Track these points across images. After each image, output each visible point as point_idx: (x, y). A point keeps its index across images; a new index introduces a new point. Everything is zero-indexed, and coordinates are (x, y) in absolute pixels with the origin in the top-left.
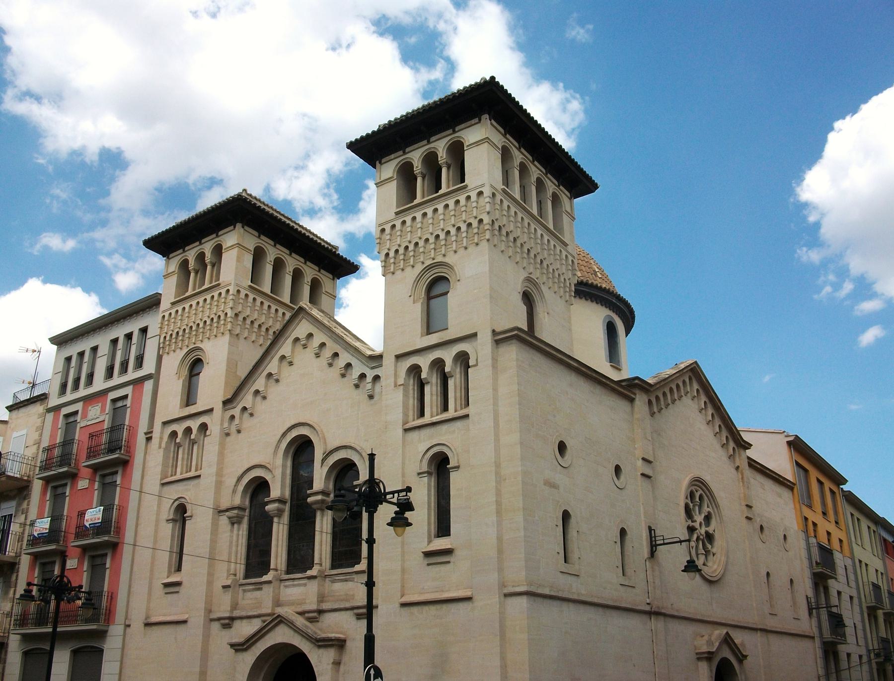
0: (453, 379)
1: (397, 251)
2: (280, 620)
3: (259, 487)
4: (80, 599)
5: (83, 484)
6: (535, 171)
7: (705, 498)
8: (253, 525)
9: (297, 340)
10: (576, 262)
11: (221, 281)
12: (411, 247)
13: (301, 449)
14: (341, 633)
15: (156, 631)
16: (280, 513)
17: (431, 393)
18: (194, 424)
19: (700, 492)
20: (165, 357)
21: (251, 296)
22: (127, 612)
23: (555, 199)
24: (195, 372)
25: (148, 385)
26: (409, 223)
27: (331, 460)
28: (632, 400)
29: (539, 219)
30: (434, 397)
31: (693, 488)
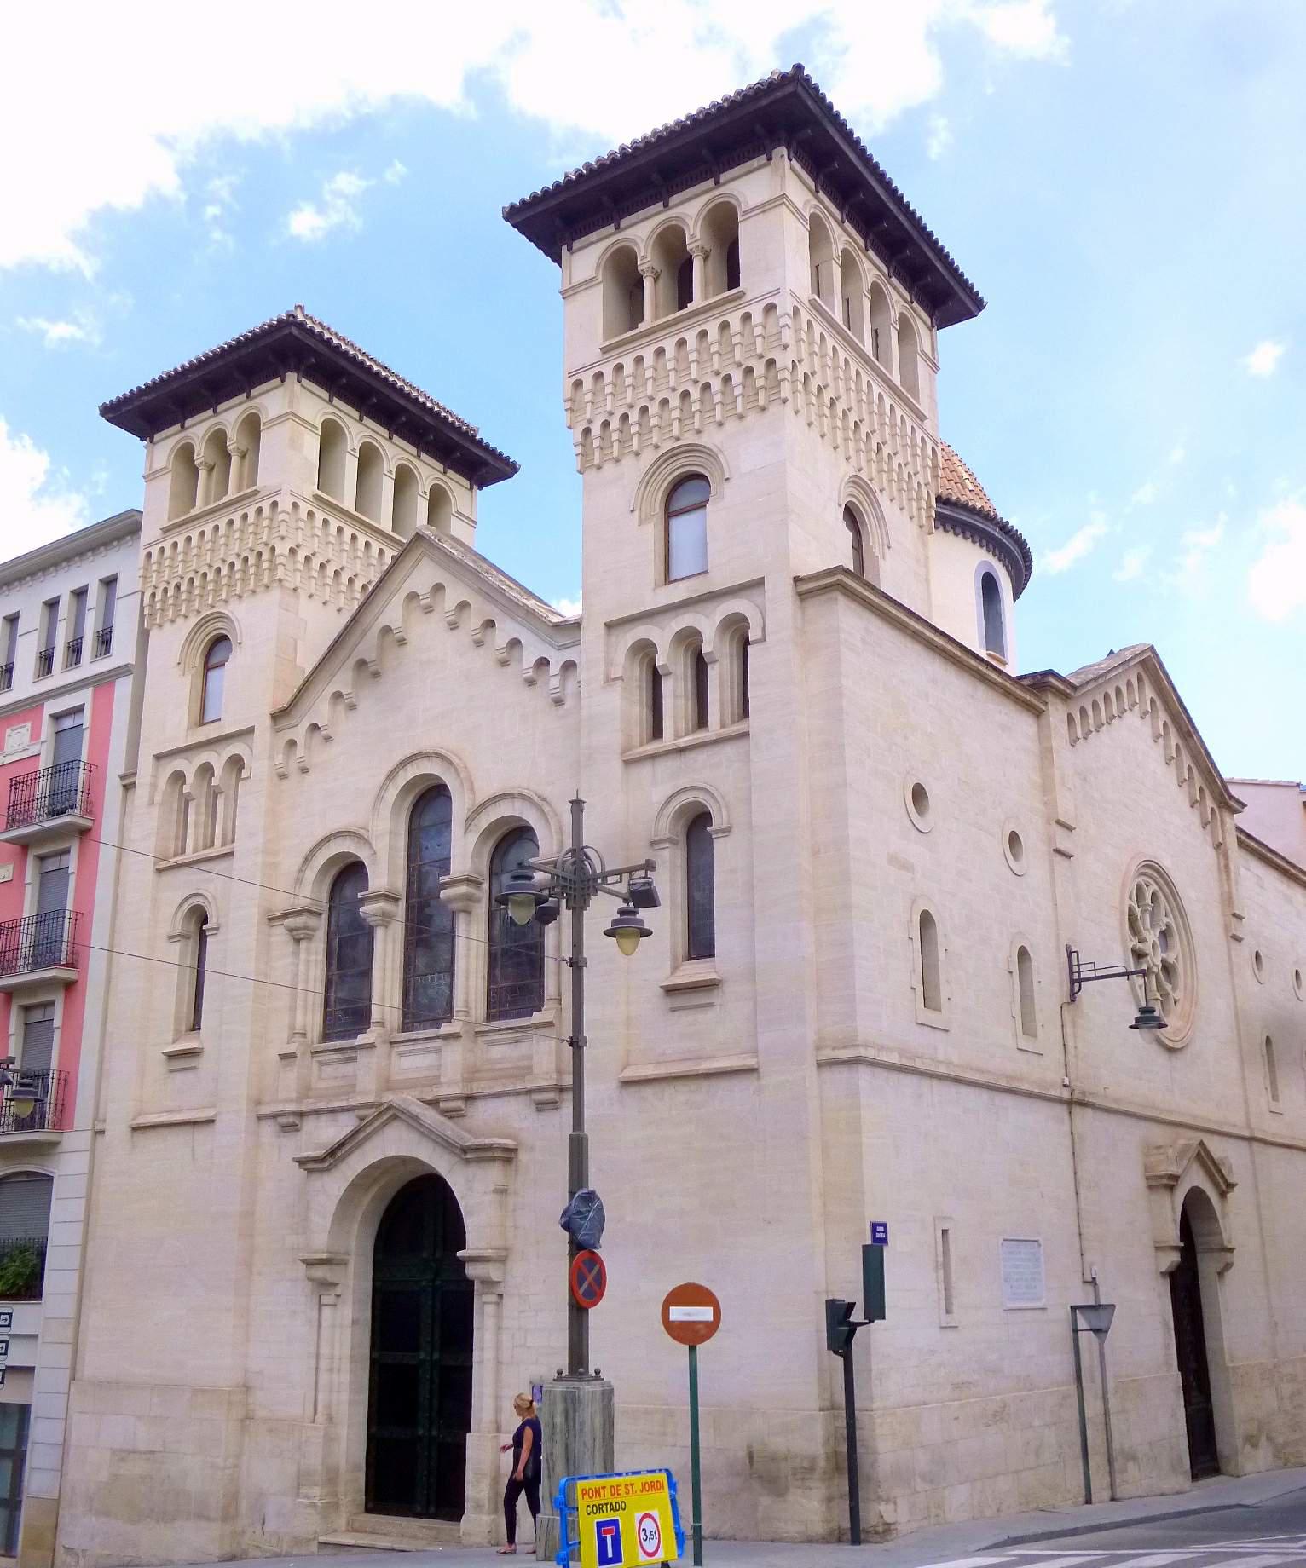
0: (717, 666)
1: (606, 424)
2: (391, 1114)
3: (349, 872)
4: (9, 1082)
6: (871, 268)
7: (1162, 898)
8: (335, 943)
9: (413, 596)
10: (938, 450)
11: (260, 483)
12: (634, 416)
13: (428, 801)
15: (153, 1141)
16: (387, 918)
17: (676, 695)
19: (1154, 887)
20: (154, 633)
21: (320, 516)
22: (97, 1108)
23: (905, 327)
24: (214, 660)
25: (123, 689)
26: (629, 368)
27: (485, 820)
28: (1038, 713)
29: (874, 363)
30: (681, 702)
31: (1142, 879)
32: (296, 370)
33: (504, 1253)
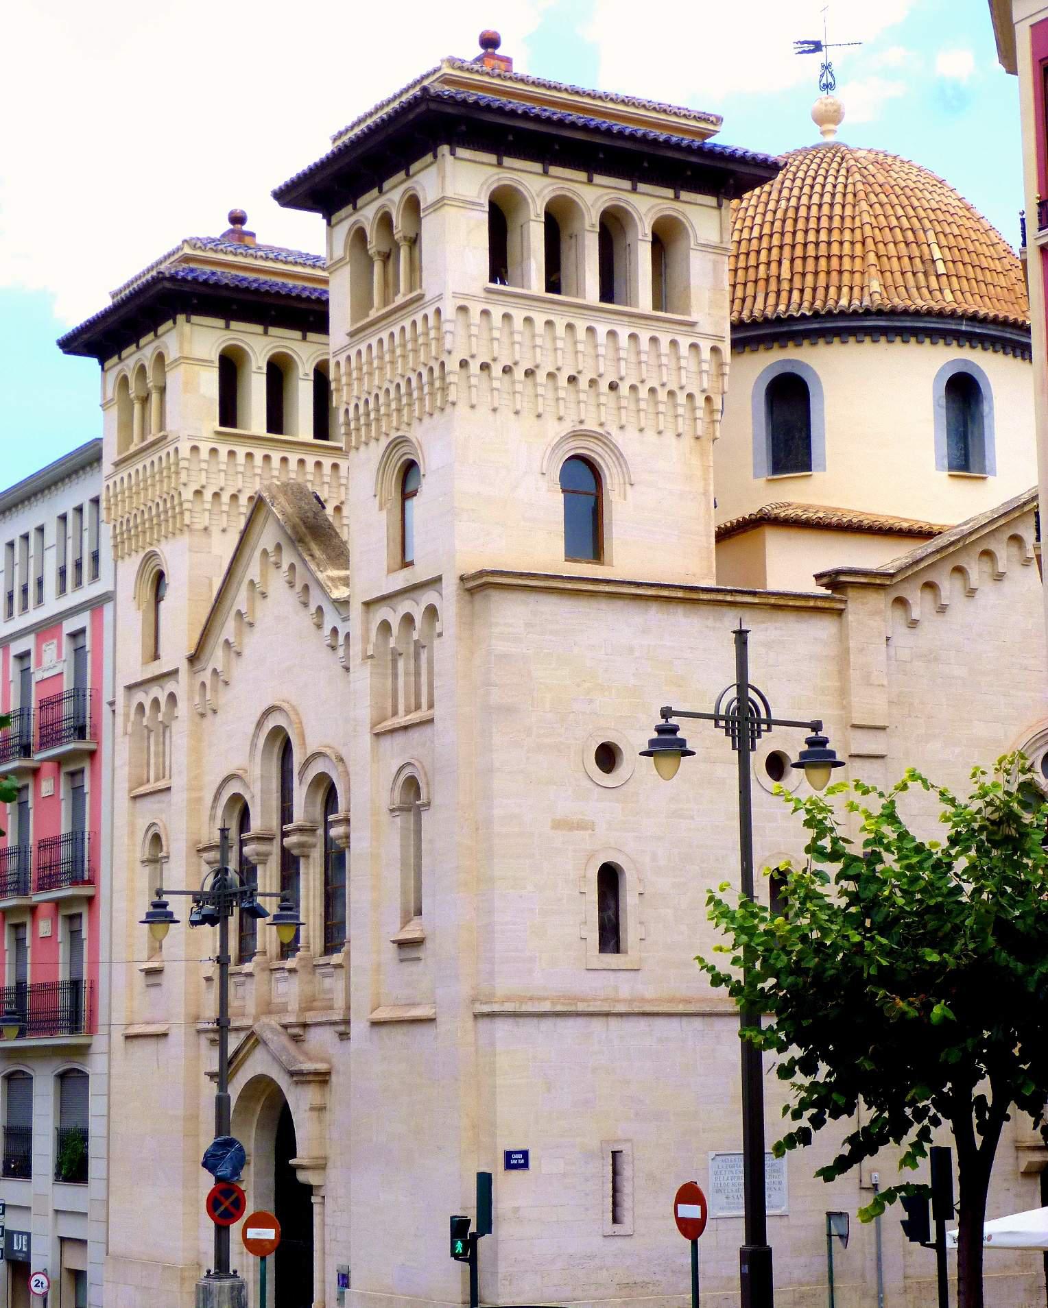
0: (426, 650)
5: (46, 787)
14: (322, 1060)
16: (264, 857)
18: (157, 692)
24: (409, 489)
32: (182, 312)
33: (321, 1162)
